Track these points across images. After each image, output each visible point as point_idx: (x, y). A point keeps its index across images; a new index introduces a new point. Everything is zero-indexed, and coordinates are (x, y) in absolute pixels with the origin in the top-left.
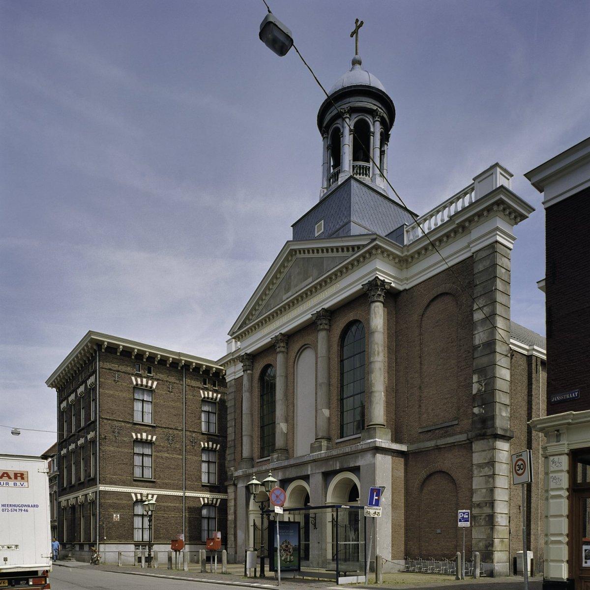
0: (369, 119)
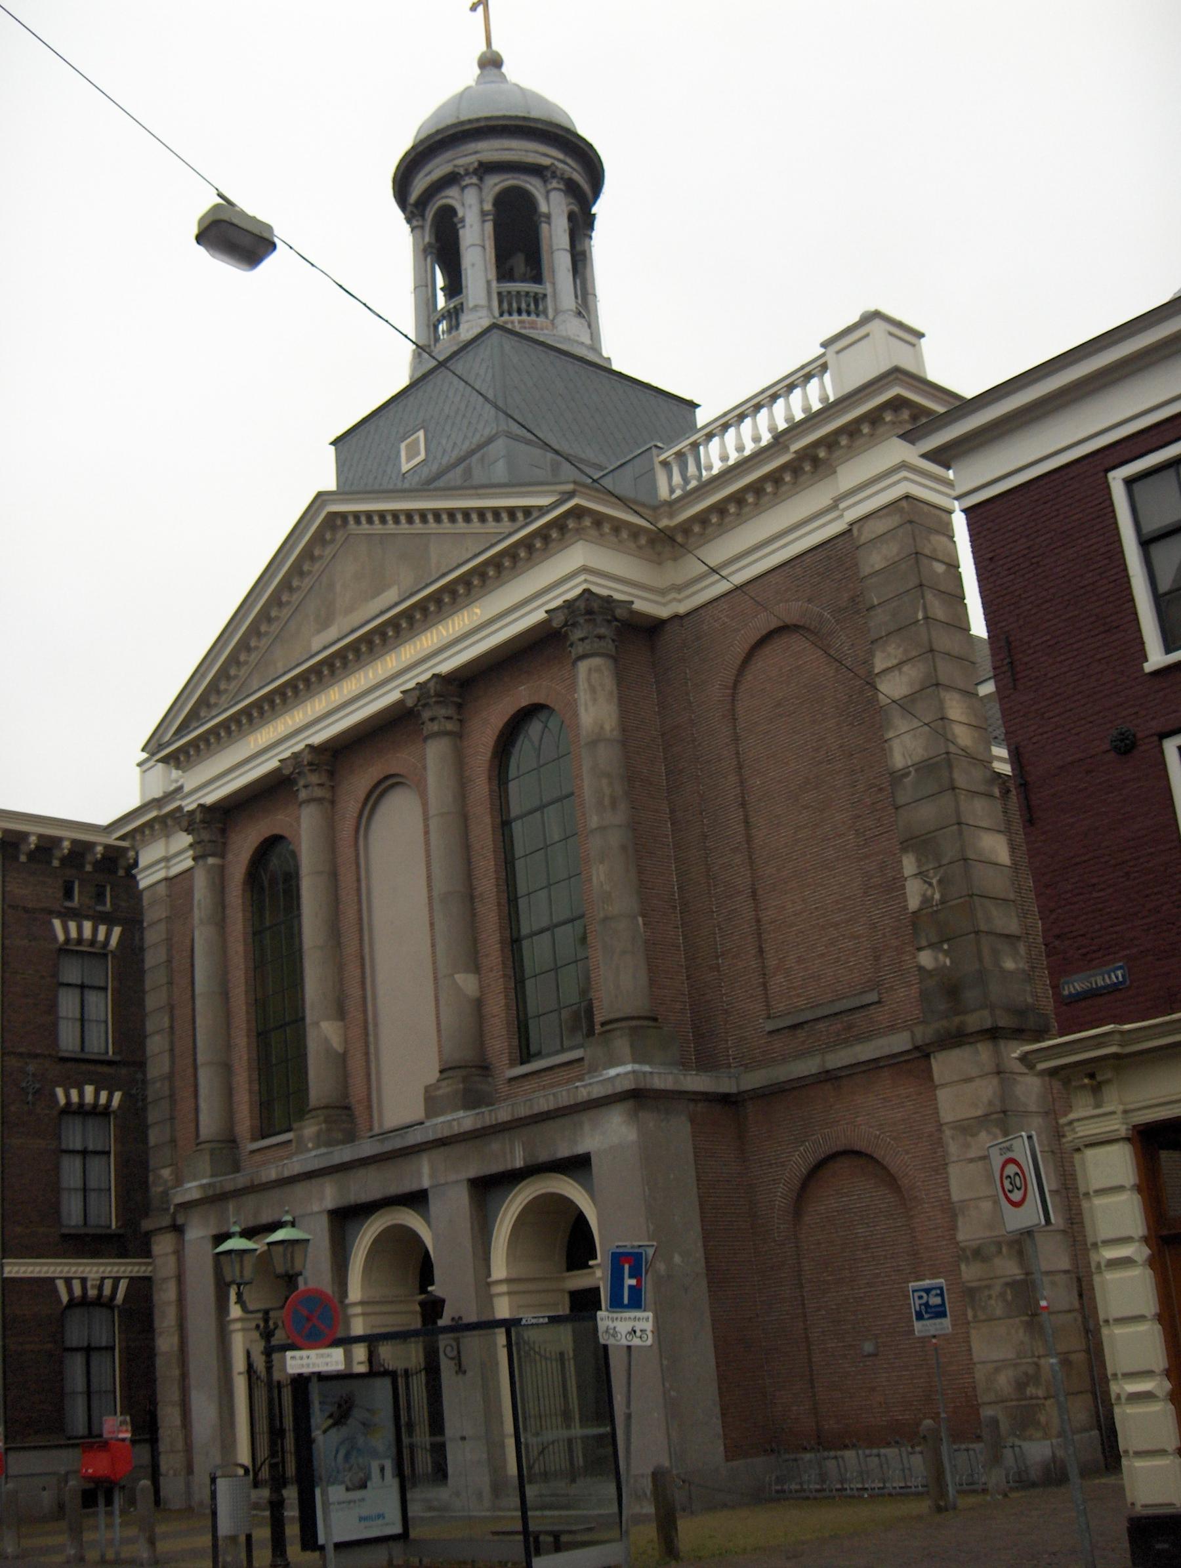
0: (533, 185)
